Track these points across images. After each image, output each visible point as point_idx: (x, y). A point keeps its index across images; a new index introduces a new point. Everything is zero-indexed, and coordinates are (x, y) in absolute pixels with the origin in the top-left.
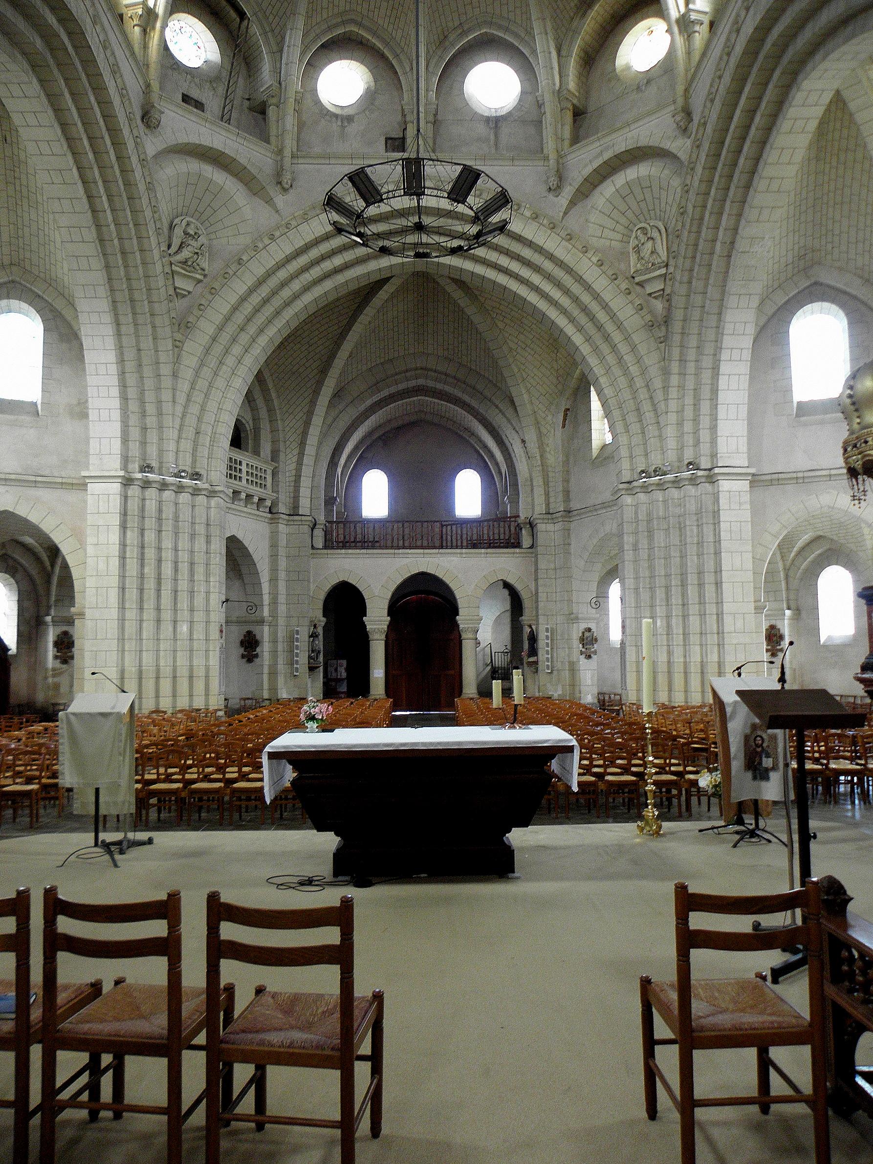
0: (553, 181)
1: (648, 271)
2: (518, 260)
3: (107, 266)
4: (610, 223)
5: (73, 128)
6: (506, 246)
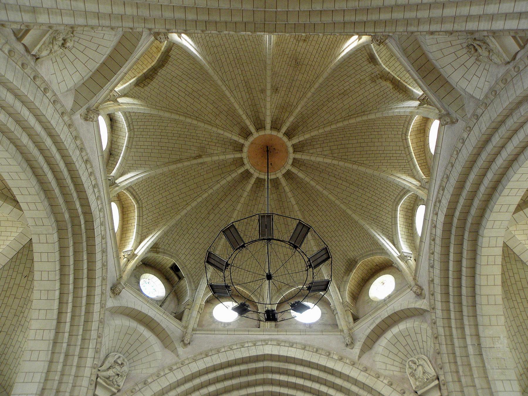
0: (348, 340)
1: (425, 384)
2: (333, 388)
3: (51, 362)
4: (389, 361)
5: (67, 269)
6: (325, 378)
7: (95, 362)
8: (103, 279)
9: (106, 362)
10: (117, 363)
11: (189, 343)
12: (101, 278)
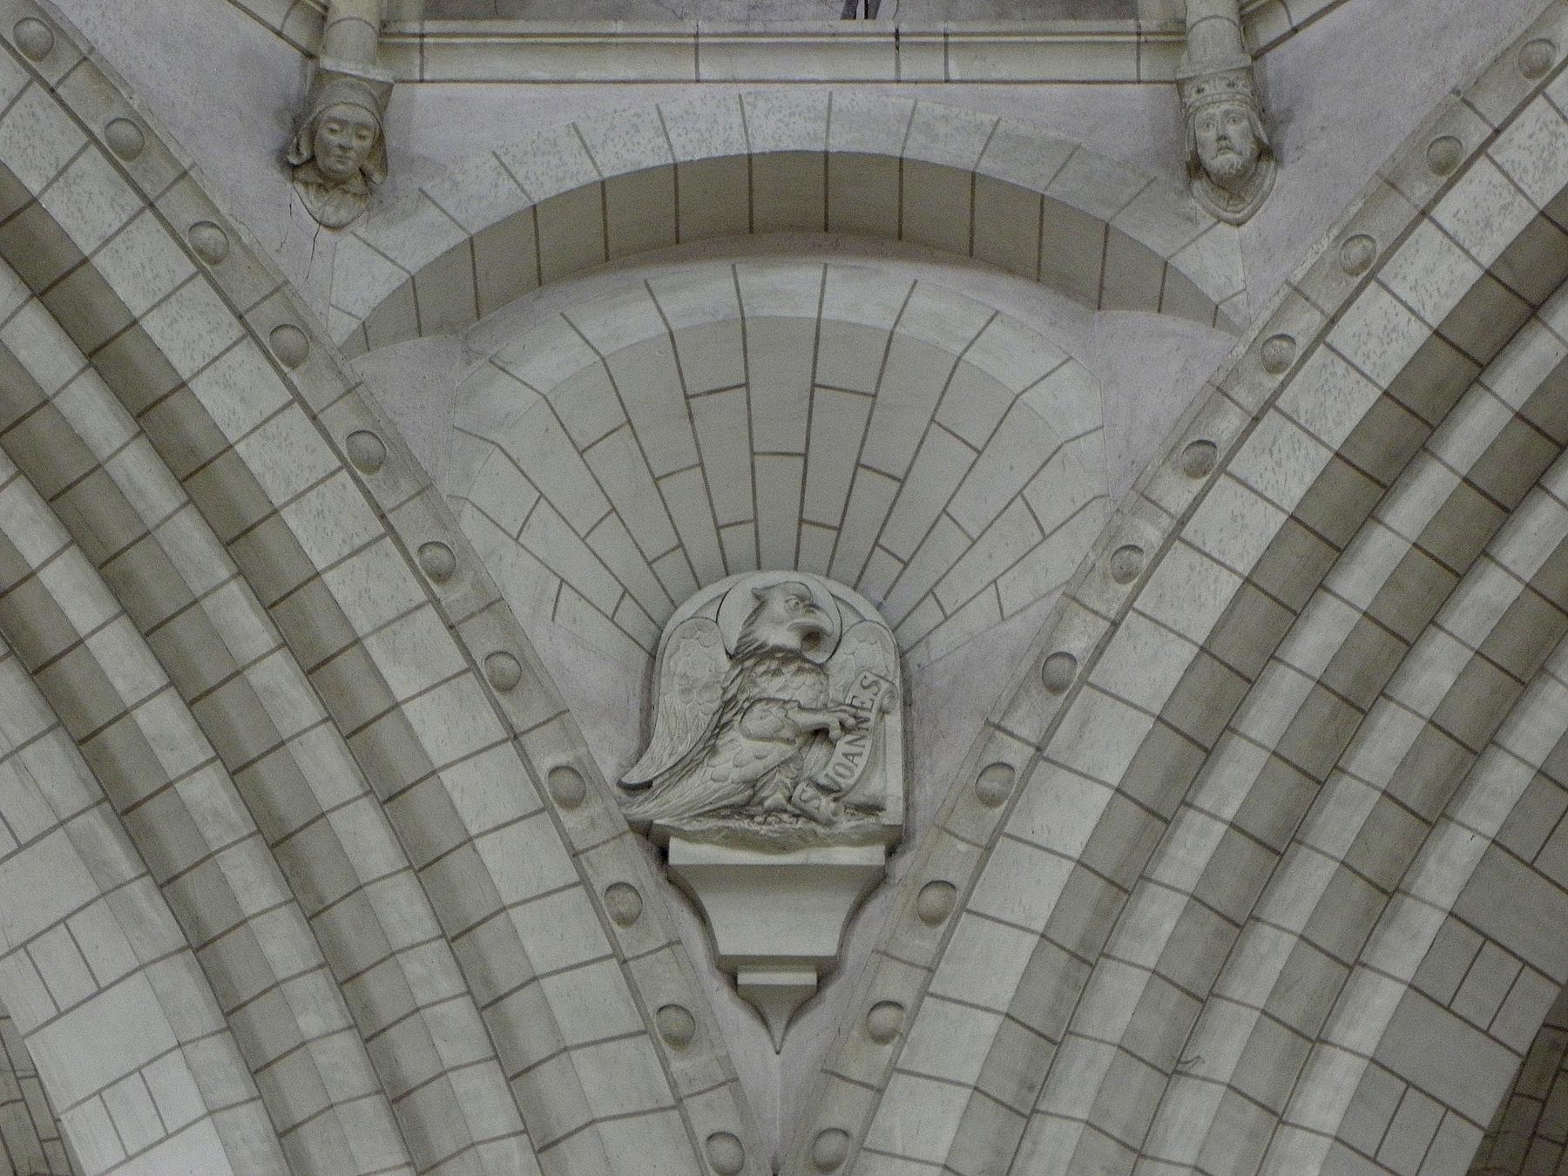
7: (545, 763)
8: (129, 150)
9: (670, 699)
10: (764, 653)
11: (1266, 152)
12: (93, 165)
